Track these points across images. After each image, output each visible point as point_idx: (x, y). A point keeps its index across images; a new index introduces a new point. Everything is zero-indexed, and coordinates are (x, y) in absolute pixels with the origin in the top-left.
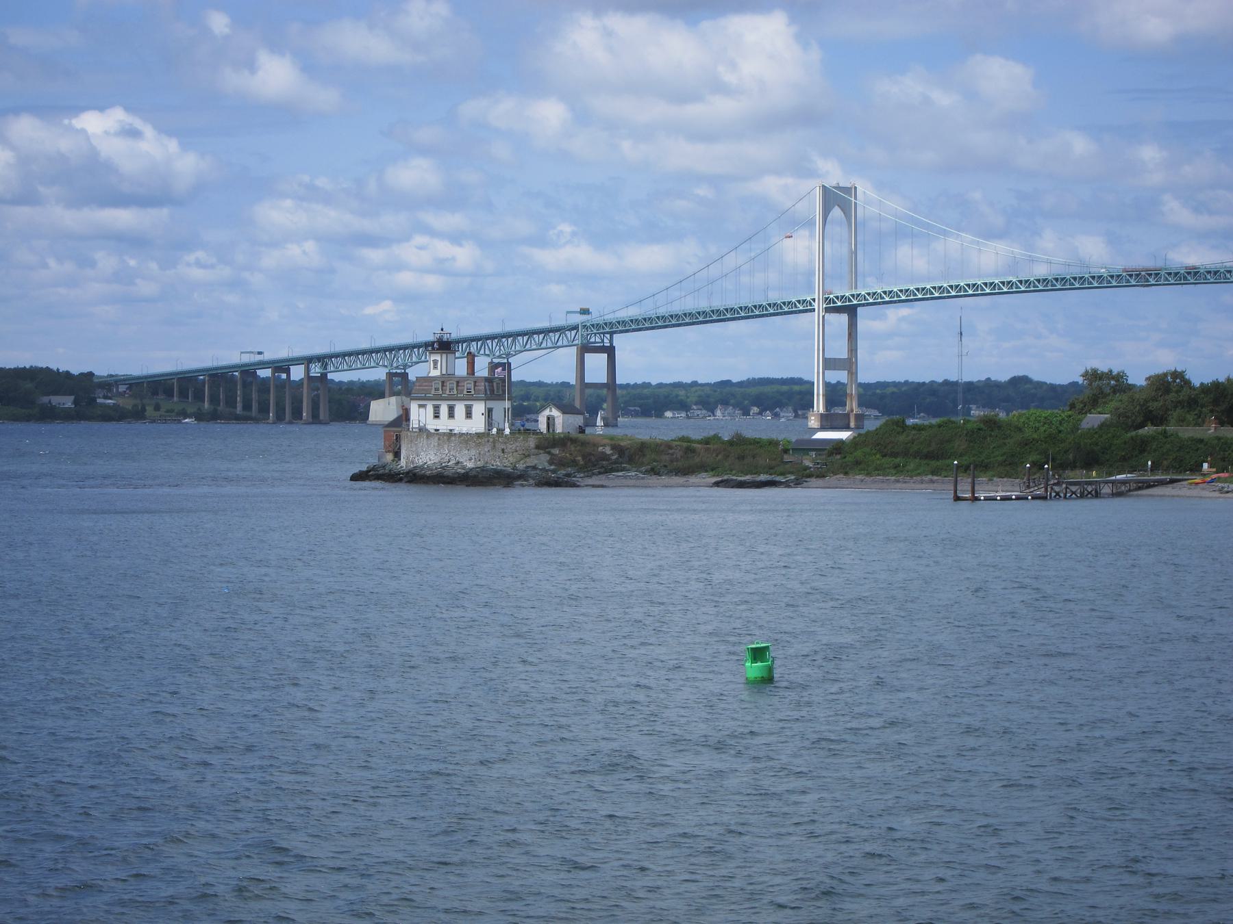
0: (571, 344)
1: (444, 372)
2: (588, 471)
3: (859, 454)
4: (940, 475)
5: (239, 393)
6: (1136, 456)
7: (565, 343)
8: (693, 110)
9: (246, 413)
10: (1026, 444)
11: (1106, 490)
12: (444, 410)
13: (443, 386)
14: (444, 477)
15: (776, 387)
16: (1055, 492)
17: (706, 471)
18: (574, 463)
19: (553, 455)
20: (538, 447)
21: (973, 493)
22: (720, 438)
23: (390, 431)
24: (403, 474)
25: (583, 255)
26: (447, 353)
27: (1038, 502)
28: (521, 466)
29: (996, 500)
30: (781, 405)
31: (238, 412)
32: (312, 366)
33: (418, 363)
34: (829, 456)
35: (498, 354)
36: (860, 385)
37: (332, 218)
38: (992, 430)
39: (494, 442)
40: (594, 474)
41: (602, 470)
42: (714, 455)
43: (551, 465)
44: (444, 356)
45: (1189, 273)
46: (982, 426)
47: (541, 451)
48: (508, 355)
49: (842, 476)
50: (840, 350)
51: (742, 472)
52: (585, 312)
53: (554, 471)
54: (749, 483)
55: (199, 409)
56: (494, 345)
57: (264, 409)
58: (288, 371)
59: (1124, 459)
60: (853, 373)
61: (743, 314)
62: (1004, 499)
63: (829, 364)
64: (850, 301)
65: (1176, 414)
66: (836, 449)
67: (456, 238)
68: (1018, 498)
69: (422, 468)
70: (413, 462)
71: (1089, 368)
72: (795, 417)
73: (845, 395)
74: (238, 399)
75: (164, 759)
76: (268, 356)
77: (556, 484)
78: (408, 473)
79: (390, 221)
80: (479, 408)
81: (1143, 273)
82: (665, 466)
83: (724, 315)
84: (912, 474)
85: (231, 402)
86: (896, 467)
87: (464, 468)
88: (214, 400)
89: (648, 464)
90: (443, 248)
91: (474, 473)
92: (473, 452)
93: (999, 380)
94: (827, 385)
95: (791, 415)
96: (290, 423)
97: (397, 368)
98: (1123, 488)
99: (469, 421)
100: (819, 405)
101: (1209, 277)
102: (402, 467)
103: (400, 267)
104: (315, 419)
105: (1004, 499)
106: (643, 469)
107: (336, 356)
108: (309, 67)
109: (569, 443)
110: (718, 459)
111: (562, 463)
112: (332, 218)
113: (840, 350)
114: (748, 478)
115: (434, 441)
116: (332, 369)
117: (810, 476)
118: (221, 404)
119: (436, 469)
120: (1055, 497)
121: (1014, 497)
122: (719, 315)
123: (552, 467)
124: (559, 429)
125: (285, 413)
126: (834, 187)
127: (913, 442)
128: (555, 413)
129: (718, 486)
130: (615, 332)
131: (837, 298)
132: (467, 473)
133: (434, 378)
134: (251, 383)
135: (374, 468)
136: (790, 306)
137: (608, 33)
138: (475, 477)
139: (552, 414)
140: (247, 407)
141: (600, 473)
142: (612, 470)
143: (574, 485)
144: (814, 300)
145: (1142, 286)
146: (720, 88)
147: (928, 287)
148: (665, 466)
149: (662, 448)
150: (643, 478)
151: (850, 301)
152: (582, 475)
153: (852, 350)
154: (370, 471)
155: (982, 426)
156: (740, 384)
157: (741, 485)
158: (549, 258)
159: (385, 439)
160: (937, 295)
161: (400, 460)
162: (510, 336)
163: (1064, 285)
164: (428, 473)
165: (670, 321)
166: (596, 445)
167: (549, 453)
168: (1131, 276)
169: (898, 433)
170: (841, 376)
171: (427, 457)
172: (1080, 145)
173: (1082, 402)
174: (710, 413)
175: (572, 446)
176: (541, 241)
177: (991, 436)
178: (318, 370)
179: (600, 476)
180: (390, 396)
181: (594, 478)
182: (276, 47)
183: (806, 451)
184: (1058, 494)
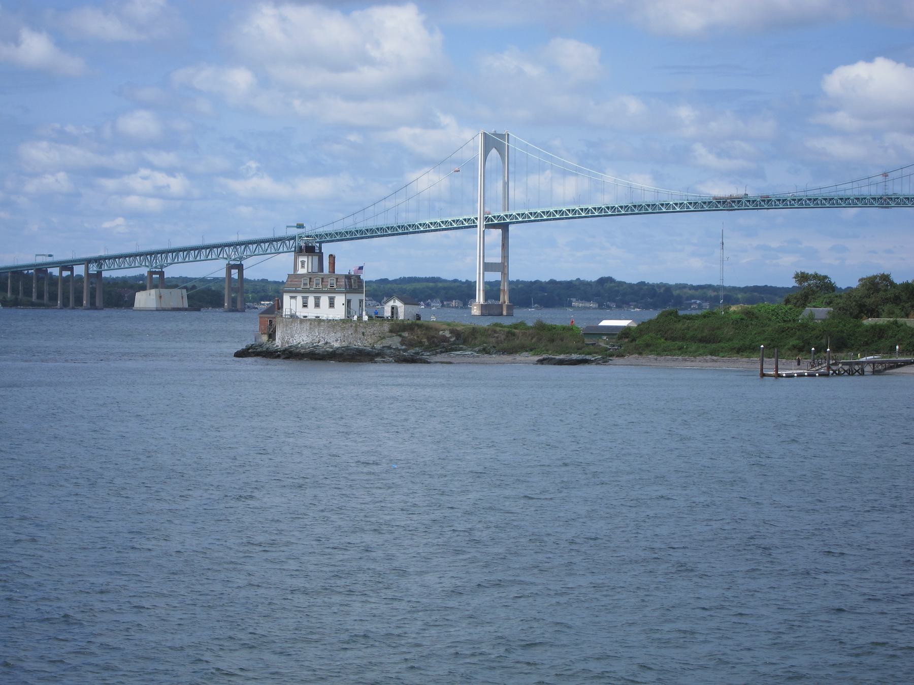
0: (289, 250)
1: (310, 271)
2: (432, 350)
3: (646, 337)
4: (718, 355)
5: (34, 285)
6: (876, 341)
7: (285, 250)
8: (346, 77)
9: (40, 301)
10: (783, 332)
11: (868, 369)
12: (311, 300)
13: (310, 281)
14: (315, 354)
15: (425, 284)
16: (833, 370)
17: (527, 351)
18: (420, 344)
19: (403, 337)
20: (391, 331)
21: (777, 371)
22: (525, 324)
23: (265, 317)
24: (280, 351)
25: (265, 185)
26: (312, 256)
27: (822, 378)
28: (378, 346)
29: (794, 376)
30: (432, 297)
31: (33, 300)
32: (91, 266)
33: (172, 264)
34: (619, 340)
35: (233, 257)
36: (511, 283)
37: (79, 155)
38: (751, 320)
39: (356, 327)
40: (437, 353)
41: (443, 350)
42: (530, 338)
43: (402, 345)
44: (310, 258)
45: (719, 202)
46: (744, 316)
47: (394, 335)
48: (241, 258)
49: (637, 355)
50: (495, 258)
51: (557, 352)
52: (300, 226)
53: (405, 351)
54: (567, 361)
55: (4, 298)
56: (231, 250)
57: (53, 298)
58: (72, 270)
59: (867, 344)
60: (505, 274)
61: (379, 234)
62: (800, 375)
63: (488, 267)
64: (504, 219)
65: (887, 307)
66: (623, 334)
67: (171, 171)
68: (809, 375)
69: (296, 347)
70: (288, 343)
71: (799, 272)
72: (442, 306)
73: (499, 290)
74: (34, 290)
75: (483, 654)
76: (58, 258)
77: (411, 360)
78: (285, 350)
79: (121, 158)
80: (340, 300)
81: (728, 201)
82: (494, 347)
83: (366, 234)
84: (695, 354)
85: (28, 293)
86: (680, 348)
87: (332, 347)
88: (15, 291)
89: (480, 345)
90: (161, 179)
91: (340, 351)
92: (339, 334)
93: (587, 280)
94: (486, 283)
95: (439, 305)
96: (73, 308)
97: (156, 267)
98: (880, 367)
99: (331, 309)
100: (480, 298)
101: (733, 205)
102: (277, 346)
103: (129, 192)
104: (93, 306)
105: (800, 375)
106: (477, 349)
107: (109, 258)
108: (61, 42)
109: (416, 328)
110: (533, 341)
111: (411, 344)
112: (79, 155)
113: (495, 258)
114: (562, 357)
115: (306, 326)
116: (106, 268)
117: (611, 355)
118: (20, 294)
119: (309, 348)
120: (832, 374)
121: (784, 375)
122: (362, 234)
123: (404, 347)
124: (401, 317)
125: (69, 301)
126: (492, 134)
127: (688, 328)
128: (398, 303)
129: (542, 364)
130: (323, 242)
131: (494, 217)
132: (334, 351)
133: (302, 276)
134: (43, 278)
135: (252, 347)
136: (414, 228)
137: (283, 19)
138: (341, 354)
139: (395, 304)
140: (40, 296)
141: (442, 352)
142: (452, 350)
143: (426, 362)
144: (477, 219)
145: (728, 210)
146: (368, 61)
147: (539, 212)
148: (494, 347)
149: (490, 332)
150: (478, 357)
151: (504, 219)
152: (428, 354)
153: (504, 257)
154: (249, 349)
155: (744, 316)
156: (395, 281)
157: (561, 362)
158: (239, 187)
159: (261, 323)
160: (520, 219)
161: (275, 340)
162: (232, 245)
163: (640, 210)
164: (302, 351)
165: (325, 238)
166: (437, 330)
167: (400, 336)
168: (719, 202)
169: (675, 322)
170: (495, 276)
171: (301, 338)
172: (634, 106)
173: (795, 298)
174: (378, 303)
175: (418, 330)
176: (235, 174)
177: (752, 324)
178: (95, 269)
179: (443, 354)
180: (150, 289)
181: (438, 355)
182: (36, 27)
183: (600, 335)
184: (834, 372)
